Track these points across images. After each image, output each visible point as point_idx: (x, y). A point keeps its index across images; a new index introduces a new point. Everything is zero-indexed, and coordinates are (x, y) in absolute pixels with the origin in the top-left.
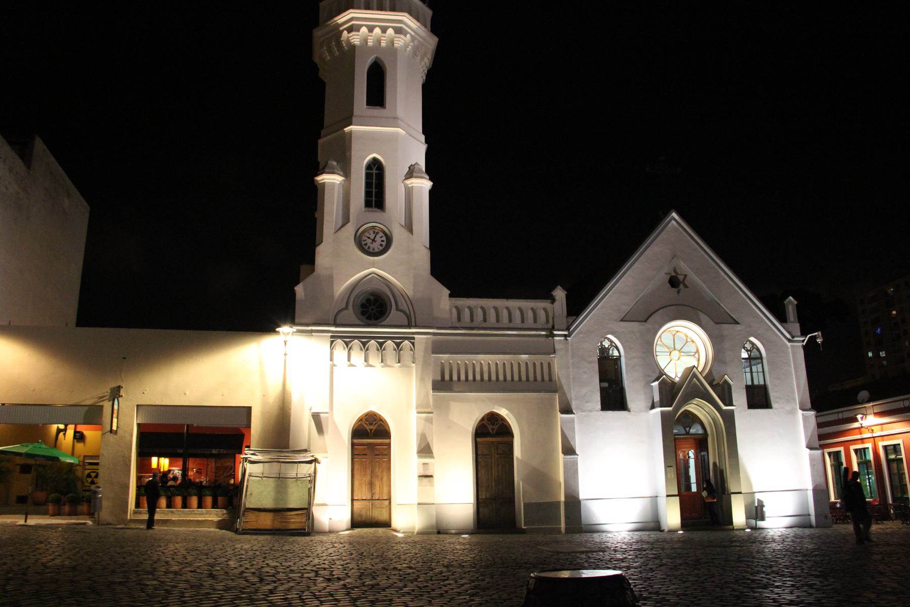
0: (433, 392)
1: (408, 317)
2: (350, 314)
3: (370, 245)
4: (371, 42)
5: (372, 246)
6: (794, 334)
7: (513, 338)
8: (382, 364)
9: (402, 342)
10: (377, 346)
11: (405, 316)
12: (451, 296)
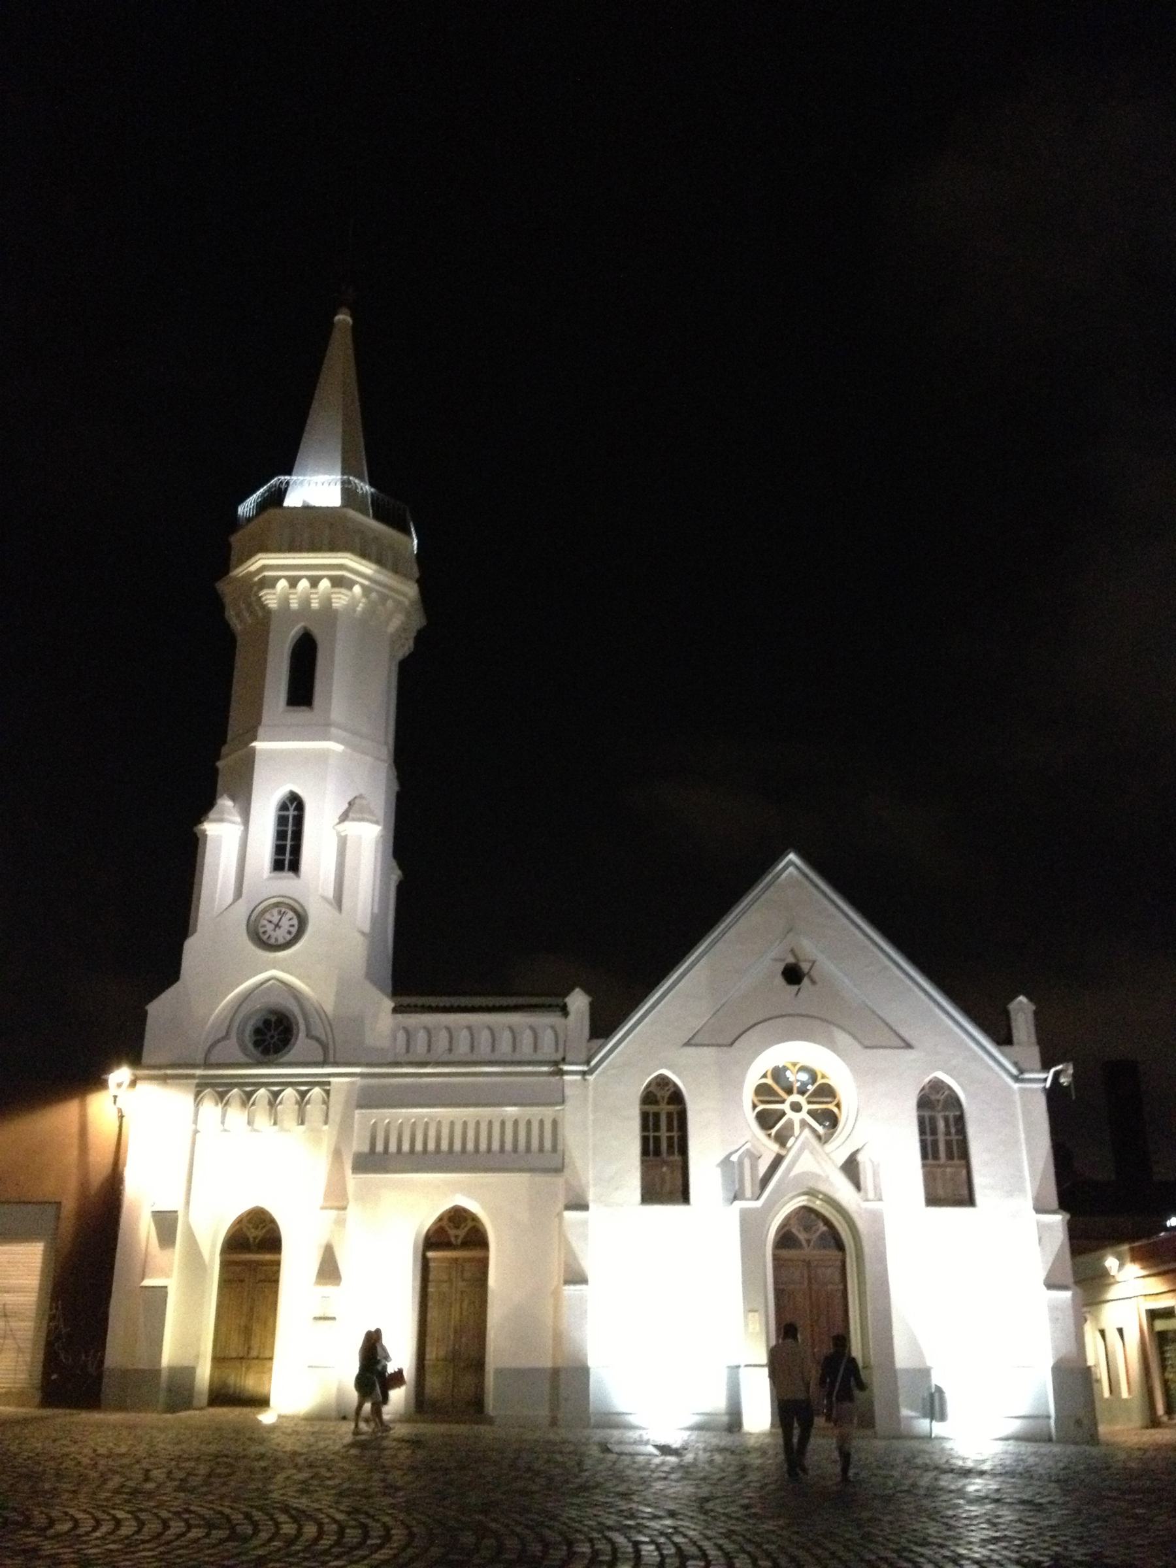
1: (325, 1048)
2: (232, 1048)
3: (272, 933)
5: (274, 935)
6: (1024, 1066)
8: (276, 1127)
9: (283, 1090)
11: (316, 1045)
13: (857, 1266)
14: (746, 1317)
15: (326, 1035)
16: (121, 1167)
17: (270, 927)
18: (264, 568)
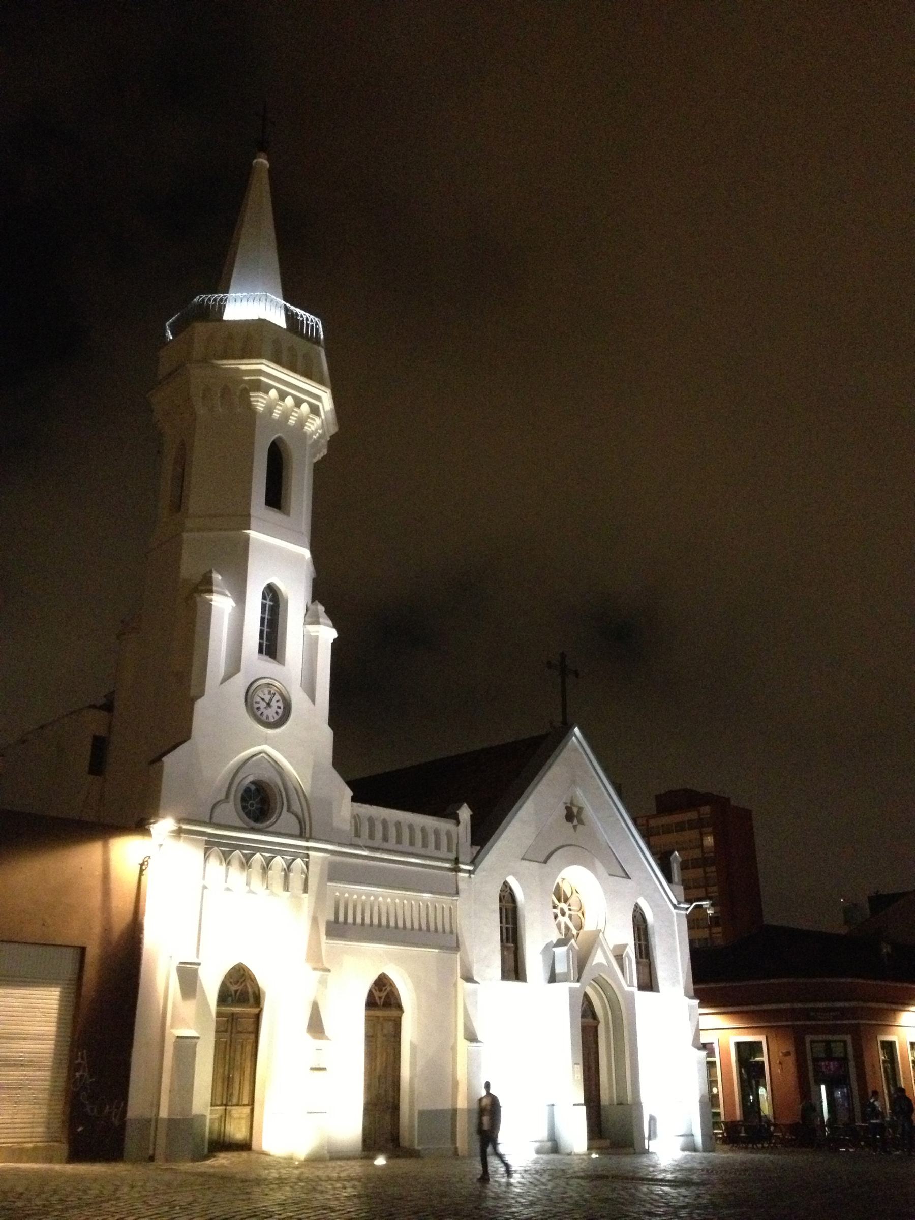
0: (326, 939)
1: (301, 822)
2: (230, 810)
3: (264, 710)
4: (278, 414)
7: (360, 861)
8: (268, 891)
10: (262, 862)
12: (354, 799)
13: (783, 1026)
14: (574, 1068)
15: (302, 810)
16: (140, 918)
17: (263, 705)
18: (260, 372)
